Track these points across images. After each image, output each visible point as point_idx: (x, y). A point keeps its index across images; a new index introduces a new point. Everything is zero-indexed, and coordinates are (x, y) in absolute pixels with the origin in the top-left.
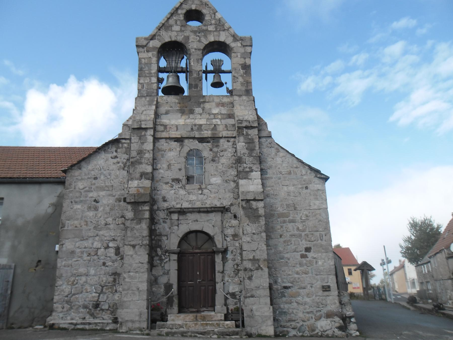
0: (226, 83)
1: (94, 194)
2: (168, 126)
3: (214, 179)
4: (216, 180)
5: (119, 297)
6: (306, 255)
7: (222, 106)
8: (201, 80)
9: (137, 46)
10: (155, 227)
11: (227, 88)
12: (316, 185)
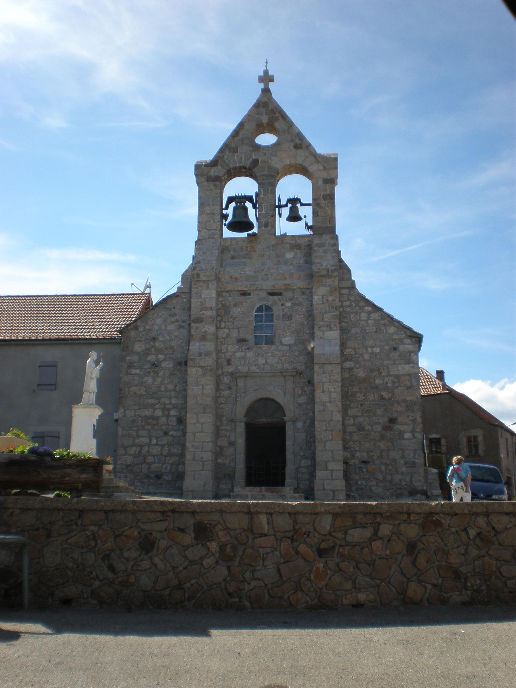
0: (305, 217)
1: (151, 358)
2: (219, 290)
3: (287, 339)
4: (288, 341)
5: (182, 468)
6: (390, 426)
7: (297, 249)
8: (274, 216)
9: (59, 437)
10: (219, 394)
11: (306, 225)
12: (407, 346)
